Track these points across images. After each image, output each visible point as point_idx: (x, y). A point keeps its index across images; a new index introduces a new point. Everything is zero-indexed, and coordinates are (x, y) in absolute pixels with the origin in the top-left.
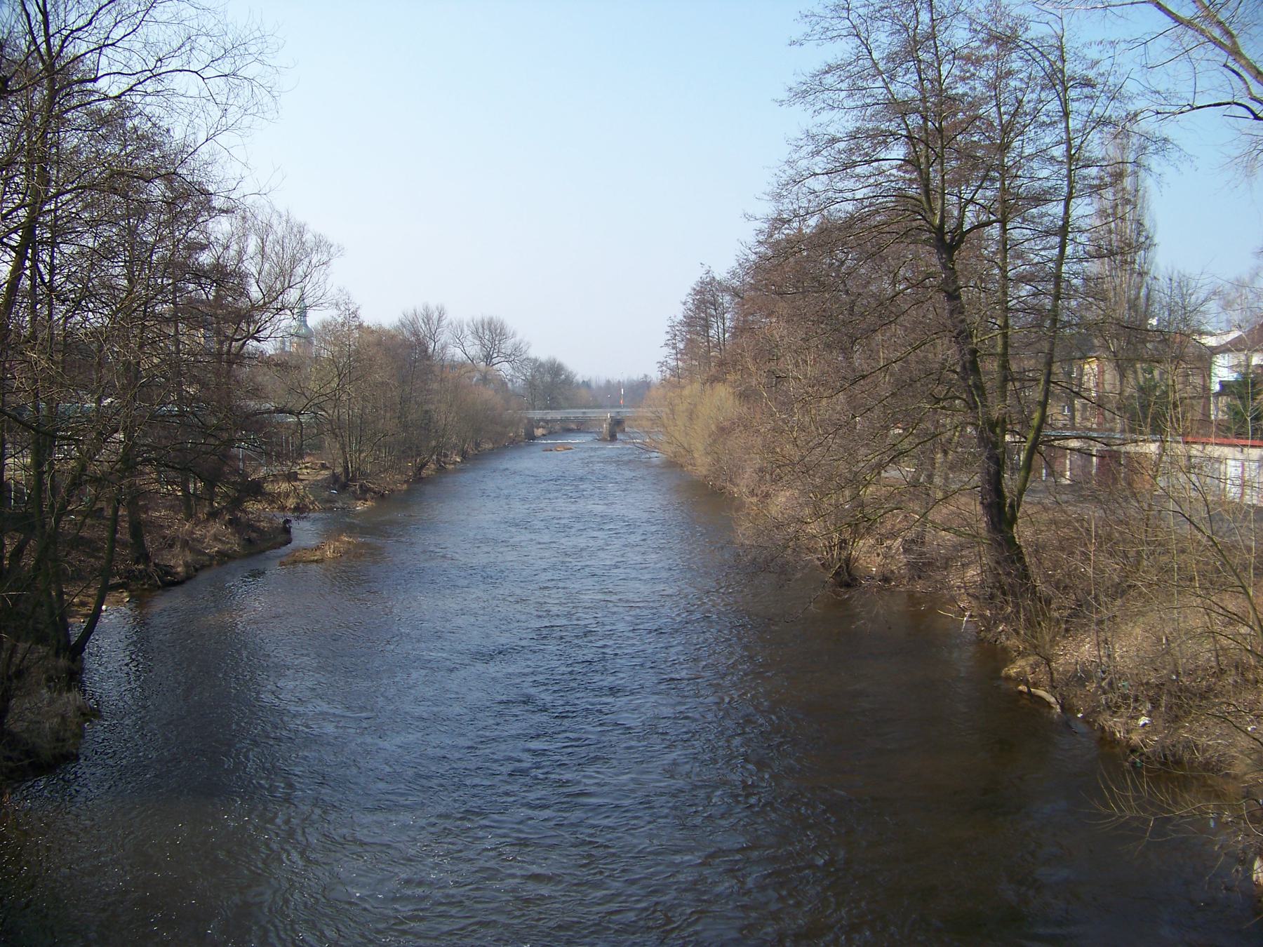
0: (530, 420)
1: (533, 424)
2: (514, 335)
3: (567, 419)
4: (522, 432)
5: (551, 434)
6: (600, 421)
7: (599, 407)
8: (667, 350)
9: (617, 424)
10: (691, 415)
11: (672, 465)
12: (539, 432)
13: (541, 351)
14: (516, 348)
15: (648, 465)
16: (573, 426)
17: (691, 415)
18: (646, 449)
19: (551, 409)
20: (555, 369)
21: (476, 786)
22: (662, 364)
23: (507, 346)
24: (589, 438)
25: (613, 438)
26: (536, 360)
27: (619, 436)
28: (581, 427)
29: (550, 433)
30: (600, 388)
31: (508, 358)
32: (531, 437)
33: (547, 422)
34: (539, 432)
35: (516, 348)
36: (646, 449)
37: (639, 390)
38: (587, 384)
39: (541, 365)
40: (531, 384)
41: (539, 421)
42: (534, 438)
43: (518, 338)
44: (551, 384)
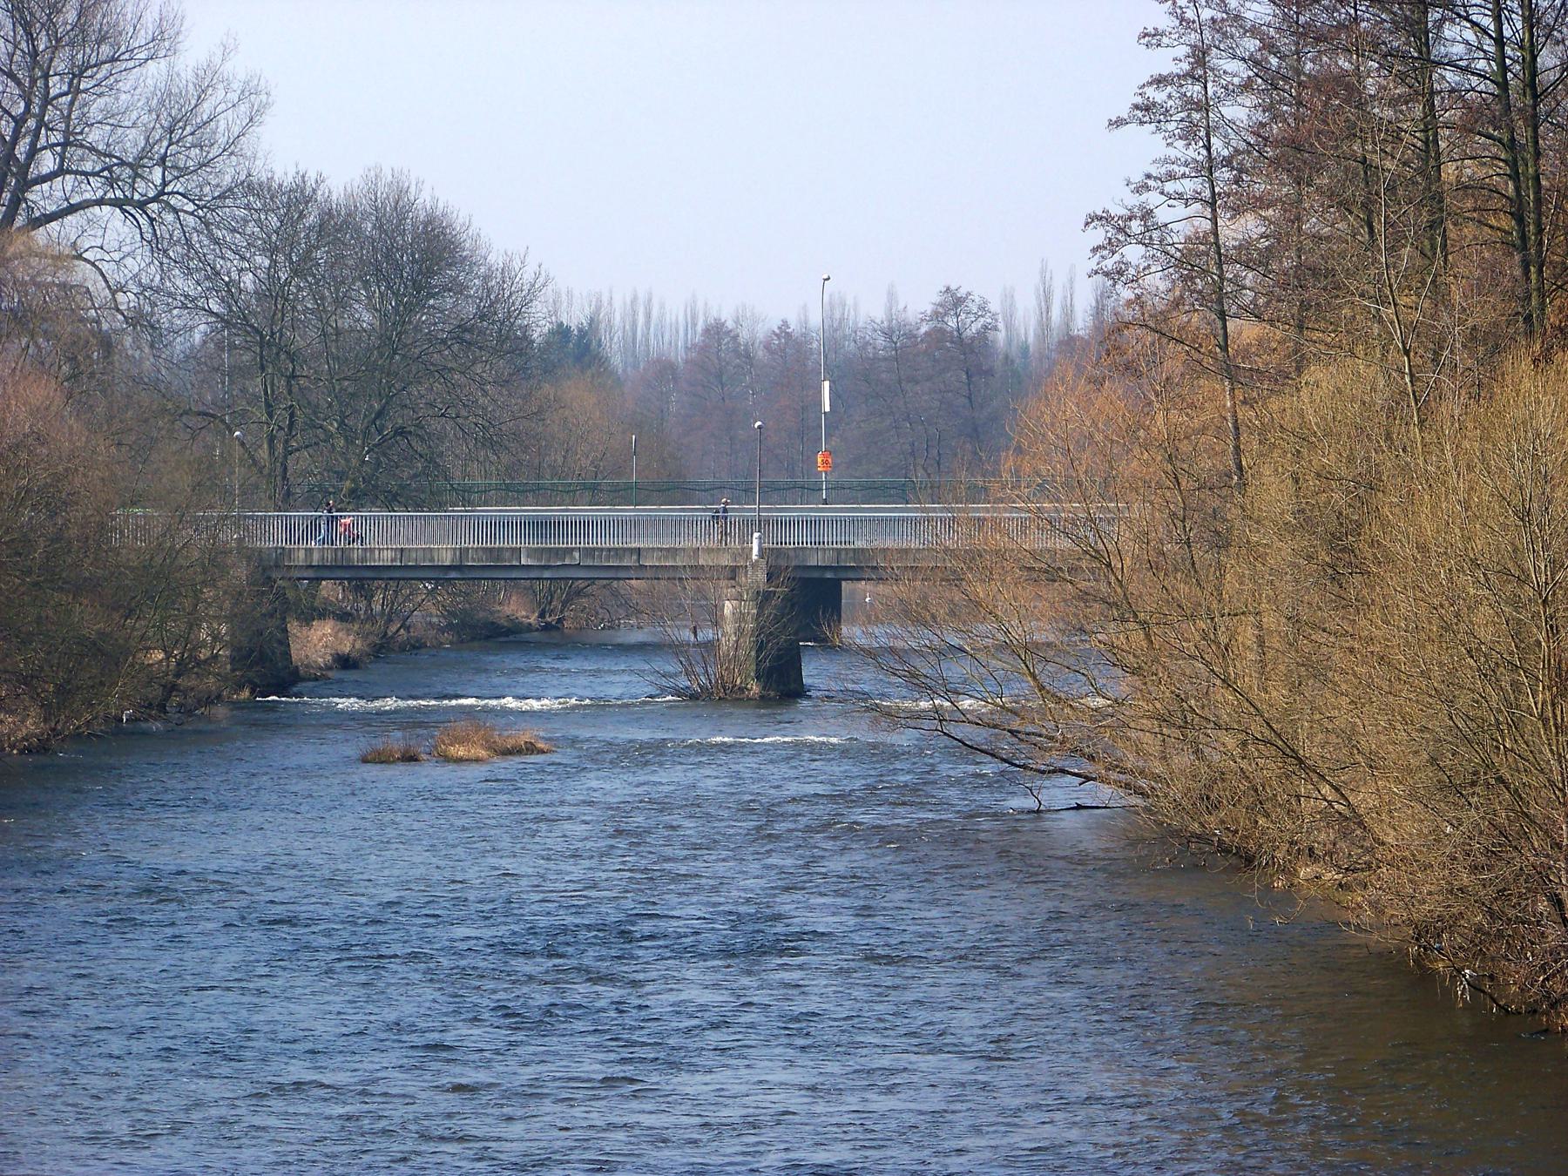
0: (268, 569)
1: (280, 593)
2: (163, 41)
3: (496, 569)
4: (214, 636)
5: (384, 655)
6: (683, 579)
7: (674, 489)
8: (1148, 147)
9: (807, 602)
10: (1342, 552)
11: (1199, 857)
12: (317, 642)
13: (322, 137)
14: (180, 122)
15: (1019, 852)
16: (516, 608)
17: (1342, 552)
18: (1015, 749)
19: (391, 500)
20: (410, 255)
21: (30, 991)
22: (1117, 228)
23: (122, 109)
24: (623, 682)
25: (782, 685)
26: (297, 199)
27: (814, 671)
28: (558, 614)
29: (382, 649)
30: (664, 370)
31: (124, 183)
32: (271, 673)
33: (362, 578)
34: (317, 642)
35: (180, 122)
36: (1015, 749)
37: (935, 396)
38: (578, 348)
39: (336, 226)
40: (258, 336)
41: (320, 572)
42: (287, 678)
43: (190, 57)
44: (386, 340)
